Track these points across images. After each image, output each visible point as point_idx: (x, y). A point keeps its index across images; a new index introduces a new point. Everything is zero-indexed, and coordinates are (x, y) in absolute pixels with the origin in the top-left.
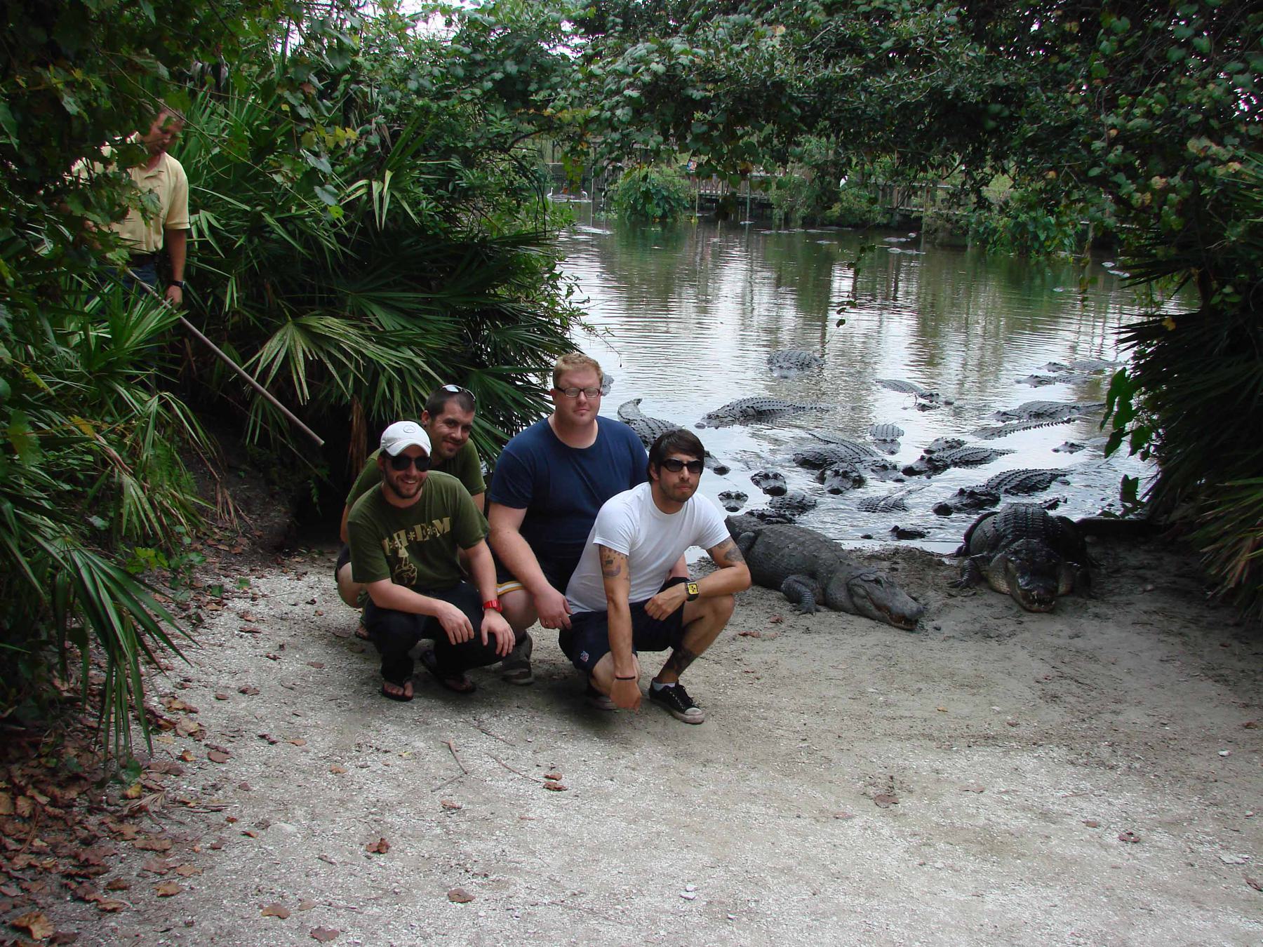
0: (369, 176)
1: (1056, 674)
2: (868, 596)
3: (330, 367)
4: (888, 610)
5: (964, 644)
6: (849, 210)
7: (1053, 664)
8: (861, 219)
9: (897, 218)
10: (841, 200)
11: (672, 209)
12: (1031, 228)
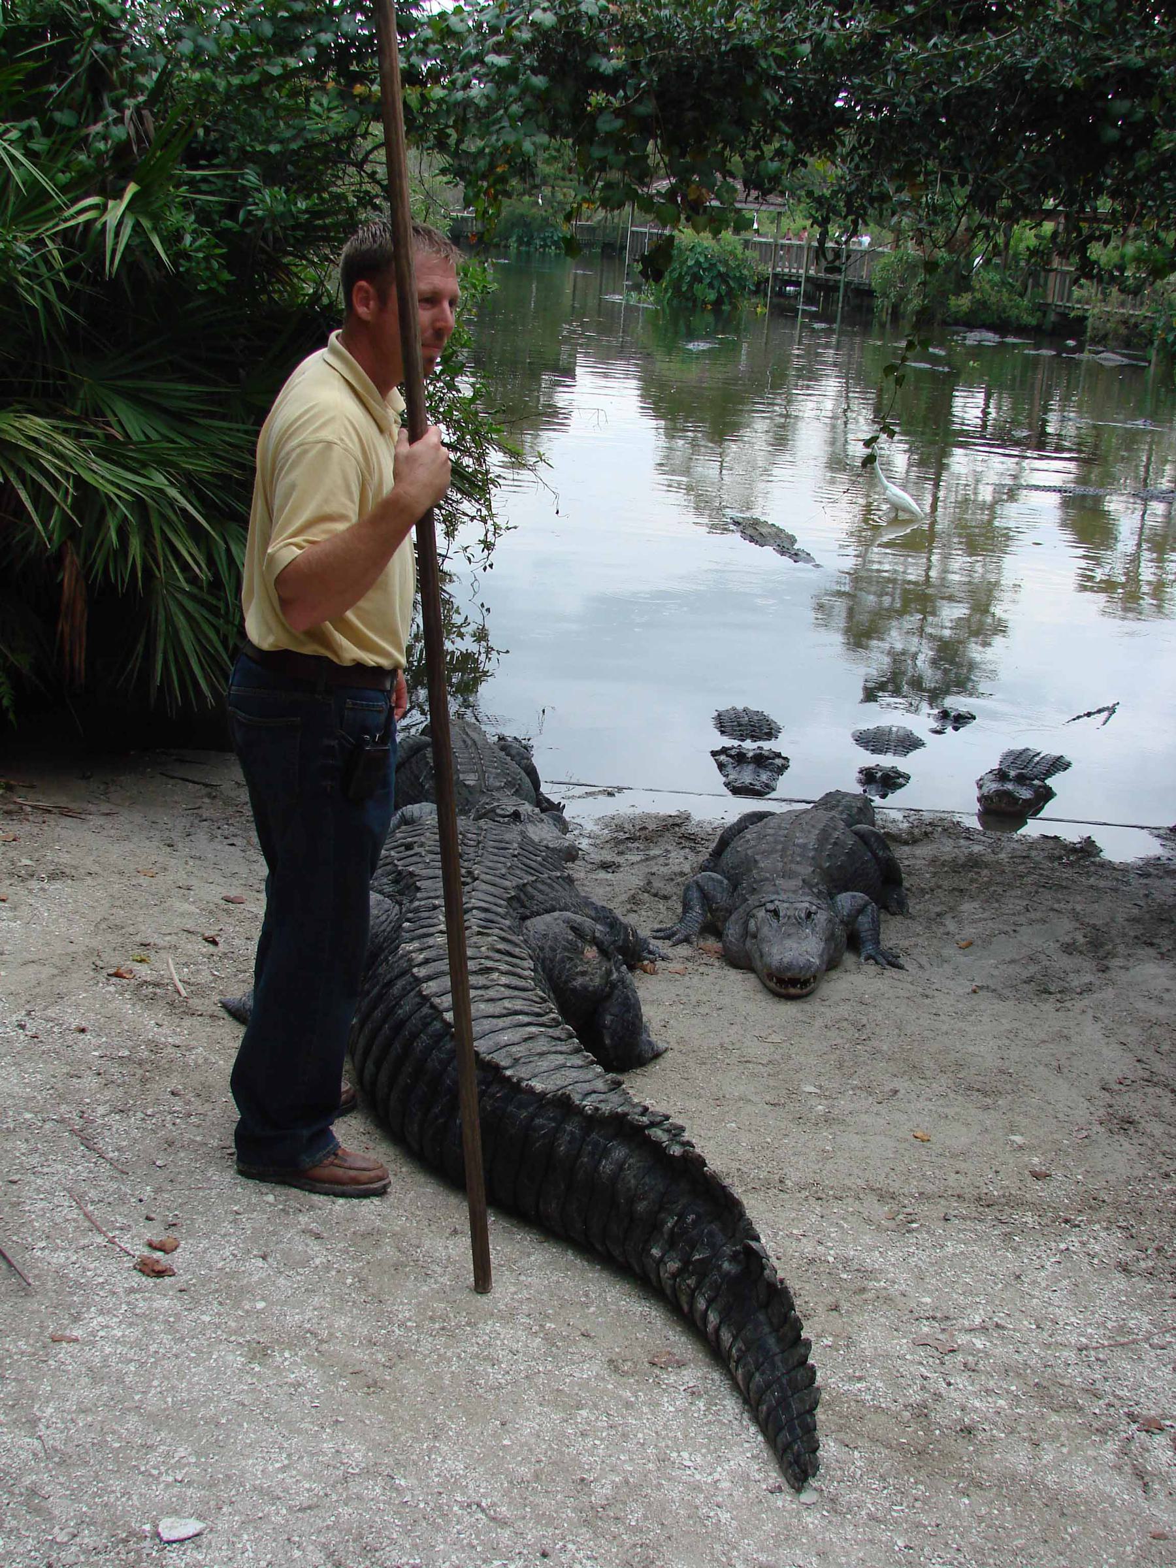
0: (103, 191)
1: (1141, 1073)
3: (23, 495)
5: (999, 1006)
6: (983, 304)
7: (1140, 1053)
8: (999, 318)
9: (1052, 317)
11: (730, 291)
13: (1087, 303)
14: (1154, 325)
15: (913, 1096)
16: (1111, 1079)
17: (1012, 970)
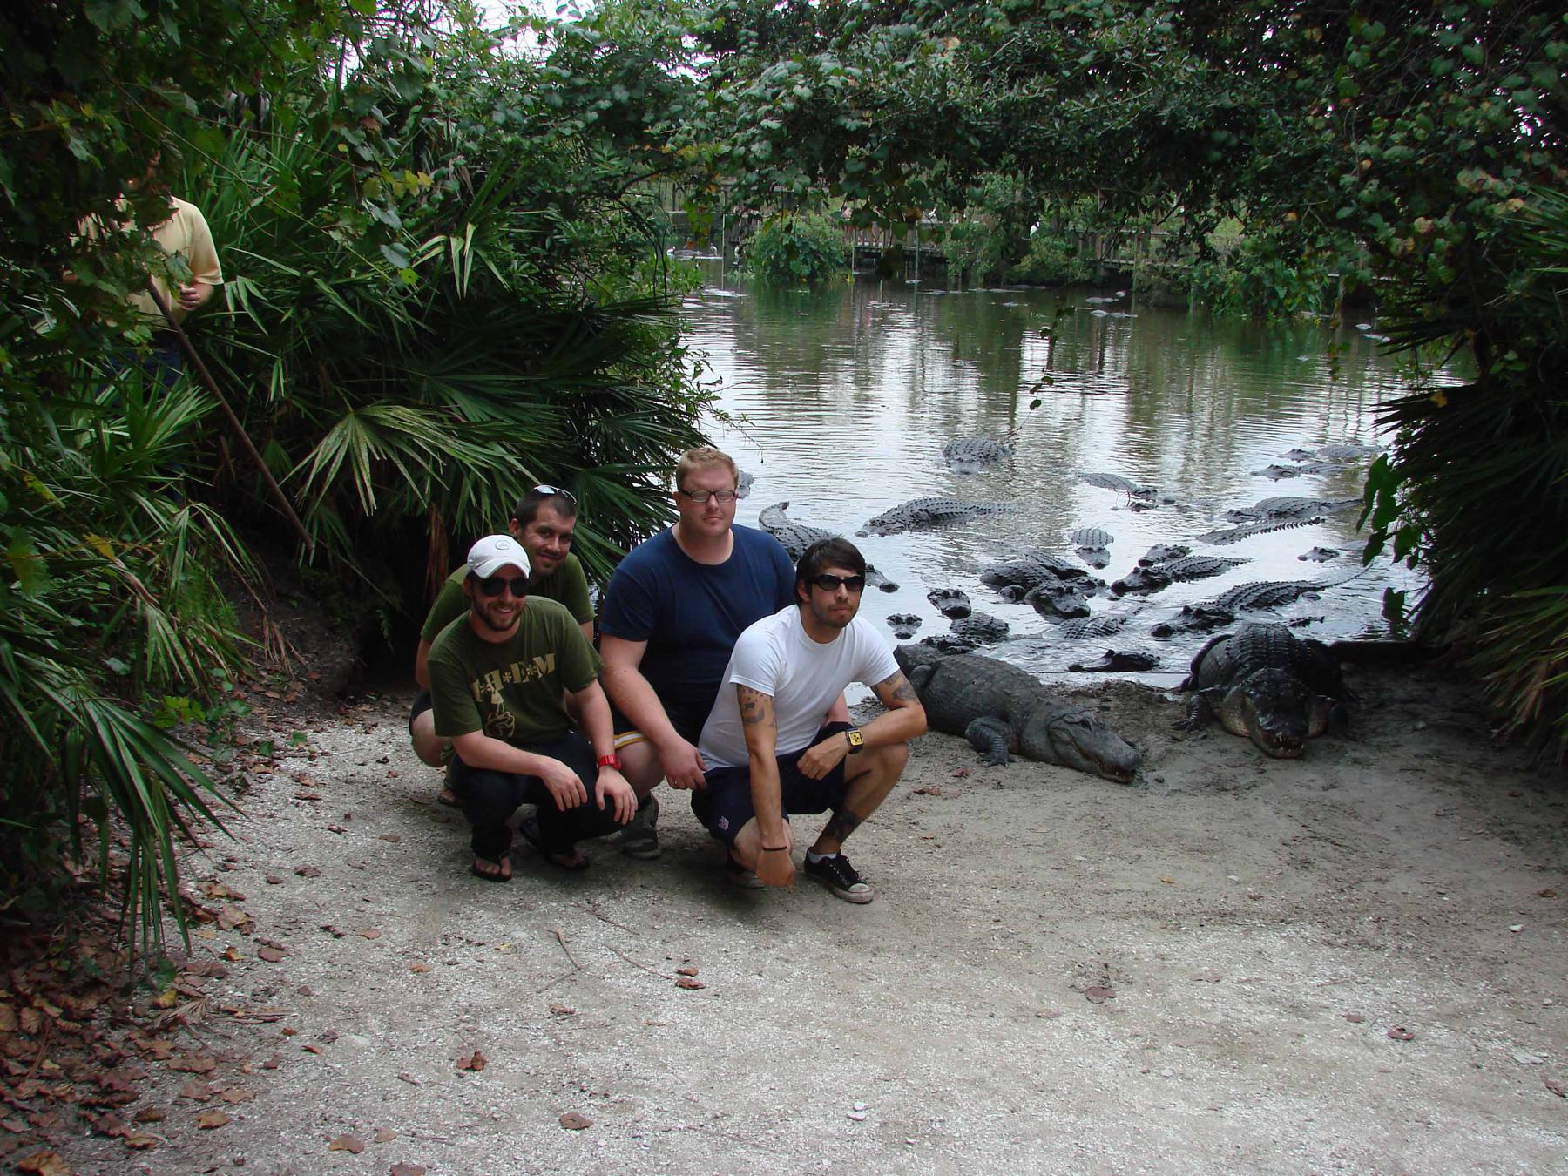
2: (1073, 741)
4: (1098, 759)
5: (1194, 799)
6: (1042, 265)
9: (1102, 273)
10: (1031, 252)
11: (822, 266)
12: (1267, 283)
13: (1132, 259)
14: (1190, 275)
15: (1153, 858)
16: (1288, 839)
17: (1191, 778)
